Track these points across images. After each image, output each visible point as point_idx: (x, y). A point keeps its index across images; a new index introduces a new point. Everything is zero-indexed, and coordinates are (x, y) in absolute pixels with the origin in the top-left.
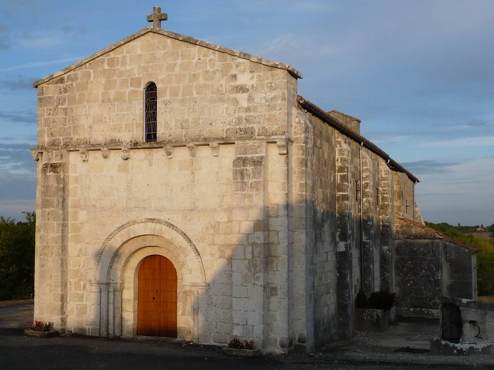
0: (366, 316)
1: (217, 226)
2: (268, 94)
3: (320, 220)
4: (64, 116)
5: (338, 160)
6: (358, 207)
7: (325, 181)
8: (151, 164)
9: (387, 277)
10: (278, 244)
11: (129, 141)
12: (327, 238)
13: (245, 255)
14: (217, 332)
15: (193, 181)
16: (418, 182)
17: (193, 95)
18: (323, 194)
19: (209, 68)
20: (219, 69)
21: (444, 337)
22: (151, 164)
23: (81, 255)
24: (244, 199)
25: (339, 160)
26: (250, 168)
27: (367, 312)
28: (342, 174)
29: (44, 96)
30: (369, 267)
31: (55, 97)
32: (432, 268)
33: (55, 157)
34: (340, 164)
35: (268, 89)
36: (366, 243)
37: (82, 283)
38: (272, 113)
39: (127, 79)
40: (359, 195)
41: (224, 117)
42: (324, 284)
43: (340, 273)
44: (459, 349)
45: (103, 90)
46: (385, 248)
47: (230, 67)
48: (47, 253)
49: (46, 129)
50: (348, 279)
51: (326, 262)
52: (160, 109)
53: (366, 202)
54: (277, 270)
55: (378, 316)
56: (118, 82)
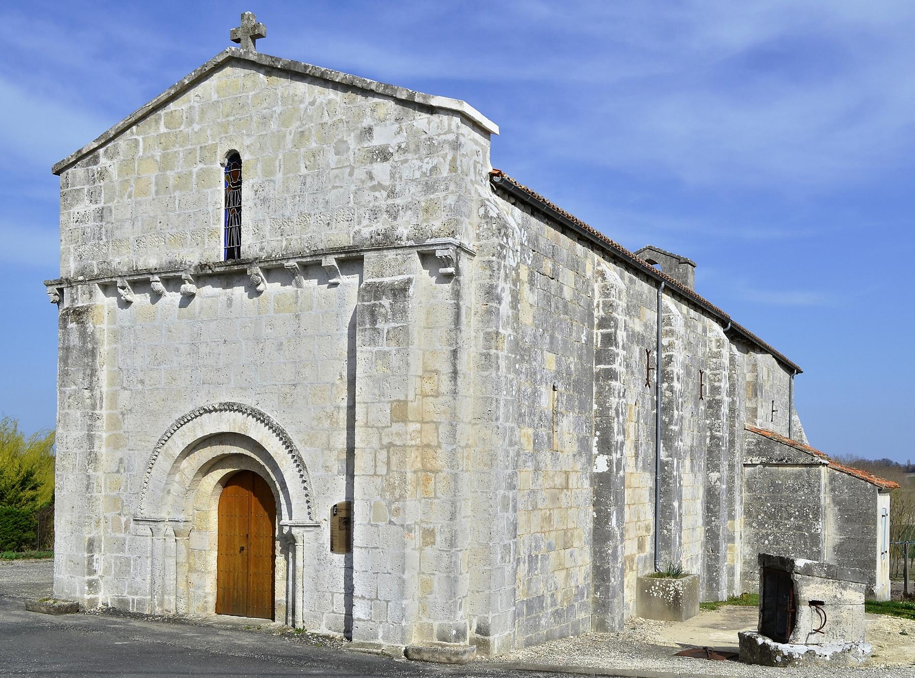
0: (656, 591)
2: (426, 160)
3: (549, 412)
4: (99, 224)
5: (598, 306)
6: (652, 399)
7: (563, 340)
9: (716, 526)
10: (437, 447)
11: (196, 263)
13: (376, 466)
15: (297, 334)
16: (799, 372)
17: (299, 171)
19: (326, 118)
20: (344, 118)
21: (763, 631)
23: (122, 471)
24: (376, 362)
25: (601, 306)
26: (386, 302)
27: (658, 583)
28: (604, 331)
29: (69, 189)
30: (669, 506)
31: (86, 190)
32: (807, 515)
33: (82, 296)
34: (602, 313)
36: (667, 463)
37: (123, 519)
38: (432, 196)
39: (195, 149)
40: (655, 377)
41: (350, 209)
42: (557, 530)
43: (598, 511)
44: (786, 654)
45: (157, 172)
46: (714, 476)
47: (361, 115)
48: (67, 466)
49: (72, 247)
50: (614, 522)
51: (562, 489)
52: (247, 200)
53: (667, 389)
54: (436, 497)
55: (676, 591)
56: (181, 155)
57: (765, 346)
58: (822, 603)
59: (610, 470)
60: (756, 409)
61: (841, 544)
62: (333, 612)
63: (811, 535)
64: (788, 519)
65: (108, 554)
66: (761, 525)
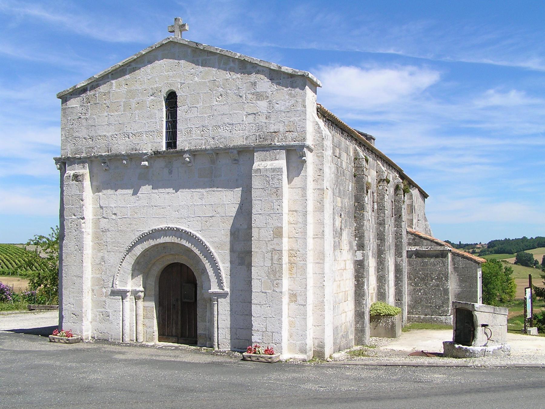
1: (236, 233)
8: (171, 172)
12: (345, 246)
14: (237, 339)
18: (342, 203)
22: (171, 172)
32: (442, 278)
35: (287, 97)
57: (416, 184)
58: (487, 325)
59: (364, 259)
60: (413, 220)
61: (459, 294)
62: (237, 339)
63: (444, 289)
64: (432, 281)
65: (95, 310)
66: (417, 285)
